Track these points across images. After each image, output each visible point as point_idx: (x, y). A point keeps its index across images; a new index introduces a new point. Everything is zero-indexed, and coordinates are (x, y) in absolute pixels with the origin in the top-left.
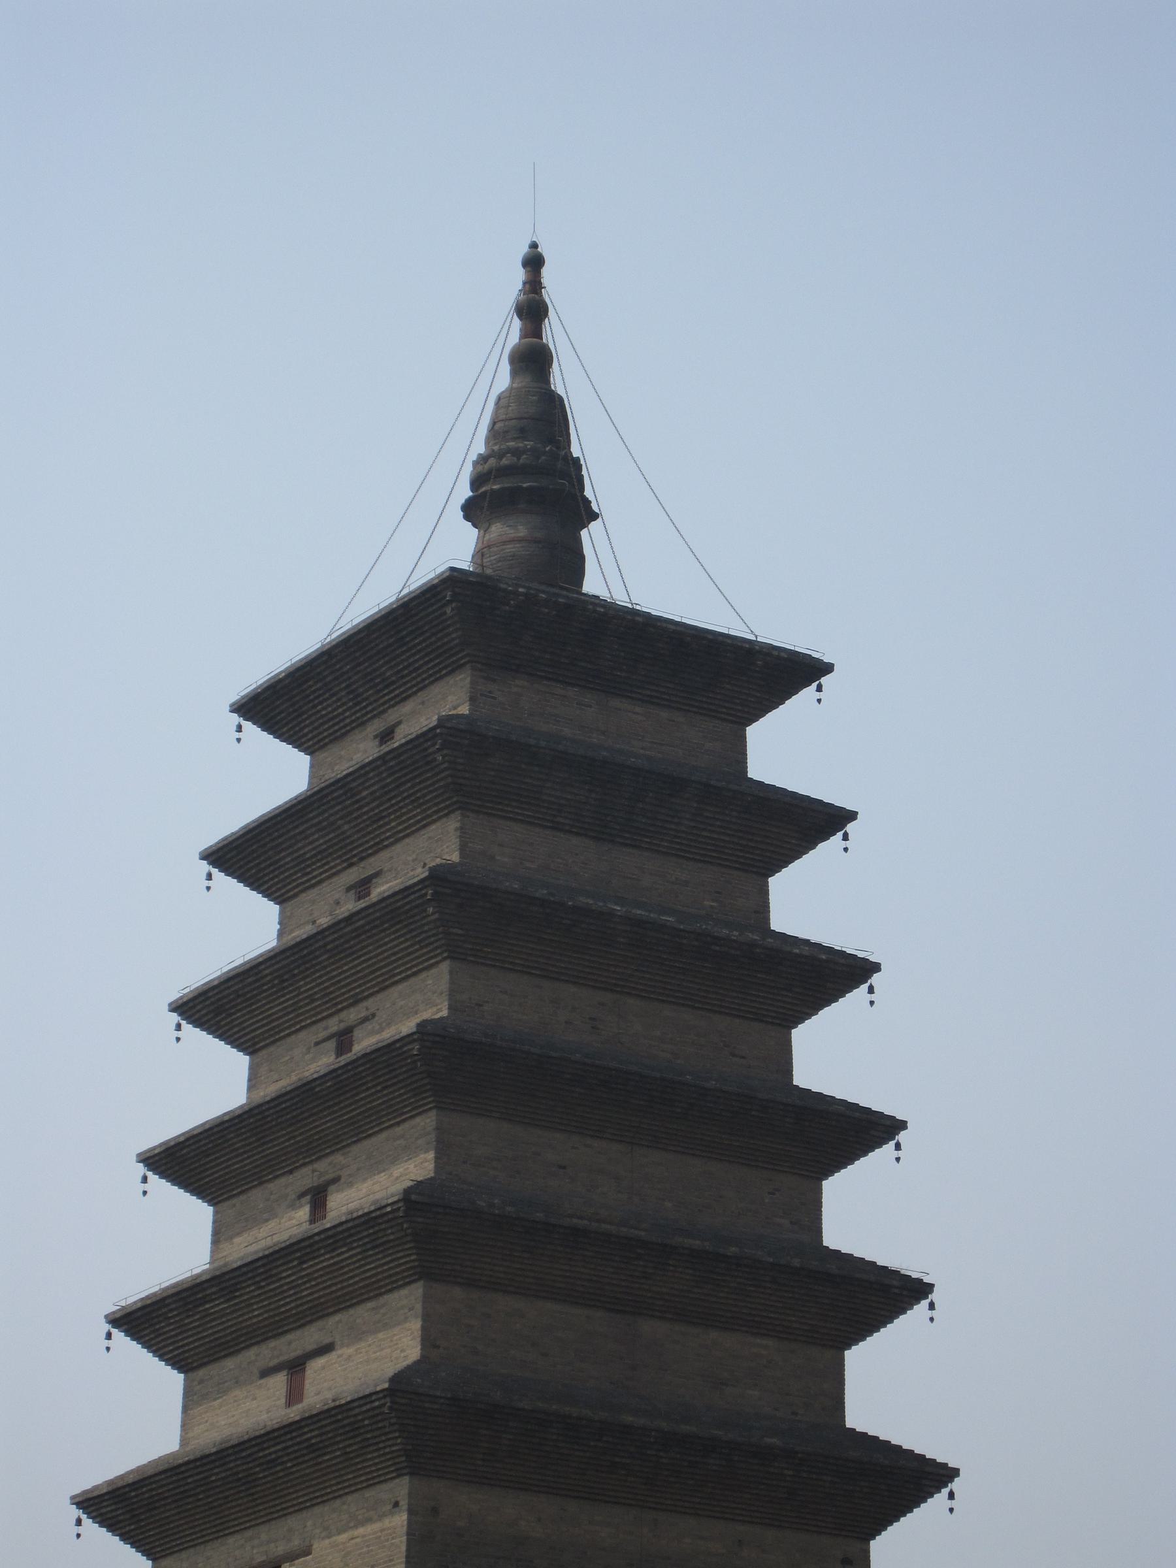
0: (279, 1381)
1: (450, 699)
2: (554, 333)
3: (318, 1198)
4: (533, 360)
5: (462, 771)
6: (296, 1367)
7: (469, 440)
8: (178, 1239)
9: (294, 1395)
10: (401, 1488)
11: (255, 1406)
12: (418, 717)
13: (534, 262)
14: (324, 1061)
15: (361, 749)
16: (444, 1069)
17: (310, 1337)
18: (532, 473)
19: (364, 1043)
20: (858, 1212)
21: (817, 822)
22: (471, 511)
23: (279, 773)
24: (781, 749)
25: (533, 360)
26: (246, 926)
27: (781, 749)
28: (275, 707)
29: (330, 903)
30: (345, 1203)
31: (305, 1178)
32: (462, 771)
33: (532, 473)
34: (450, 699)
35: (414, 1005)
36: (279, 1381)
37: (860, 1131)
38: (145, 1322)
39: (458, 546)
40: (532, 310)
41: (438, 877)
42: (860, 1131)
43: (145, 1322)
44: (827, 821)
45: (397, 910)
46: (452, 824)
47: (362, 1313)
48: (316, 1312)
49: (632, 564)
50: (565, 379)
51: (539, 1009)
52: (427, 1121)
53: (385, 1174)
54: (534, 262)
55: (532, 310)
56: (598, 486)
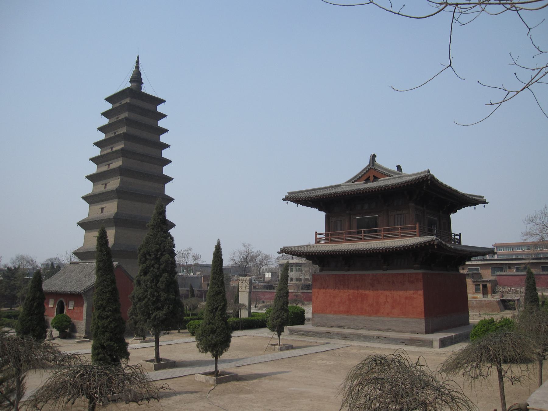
0: (107, 166)
1: (128, 100)
2: (140, 65)
3: (112, 149)
4: (137, 67)
5: (129, 107)
6: (109, 165)
7: (131, 75)
8: (93, 169)
9: (105, 187)
10: (119, 177)
11: (104, 168)
12: (124, 102)
13: (138, 57)
14: (113, 135)
15: (118, 105)
16: (126, 137)
17: (110, 162)
18: (137, 79)
19: (117, 133)
20: (165, 154)
21: (164, 116)
22: (130, 82)
23: (109, 106)
24: (160, 109)
25: (137, 67)
26: (105, 121)
27: (160, 109)
28: (109, 99)
29: (114, 120)
30: (114, 149)
31: (110, 146)
32: (129, 107)
33: (137, 79)
34: (128, 100)
35: (122, 130)
36: (107, 166)
37: (166, 146)
38: (94, 160)
39: (129, 85)
40: (138, 62)
41: (125, 118)
42: (166, 146)
43: (94, 160)
44: (165, 116)
45: (121, 120)
46: (129, 98)
47: (116, 160)
48: (111, 159)
49: (146, 89)
50: (141, 69)
51: (135, 116)
52: (123, 142)
53: (118, 147)
54: (138, 57)
55: (138, 62)
56: (143, 81)
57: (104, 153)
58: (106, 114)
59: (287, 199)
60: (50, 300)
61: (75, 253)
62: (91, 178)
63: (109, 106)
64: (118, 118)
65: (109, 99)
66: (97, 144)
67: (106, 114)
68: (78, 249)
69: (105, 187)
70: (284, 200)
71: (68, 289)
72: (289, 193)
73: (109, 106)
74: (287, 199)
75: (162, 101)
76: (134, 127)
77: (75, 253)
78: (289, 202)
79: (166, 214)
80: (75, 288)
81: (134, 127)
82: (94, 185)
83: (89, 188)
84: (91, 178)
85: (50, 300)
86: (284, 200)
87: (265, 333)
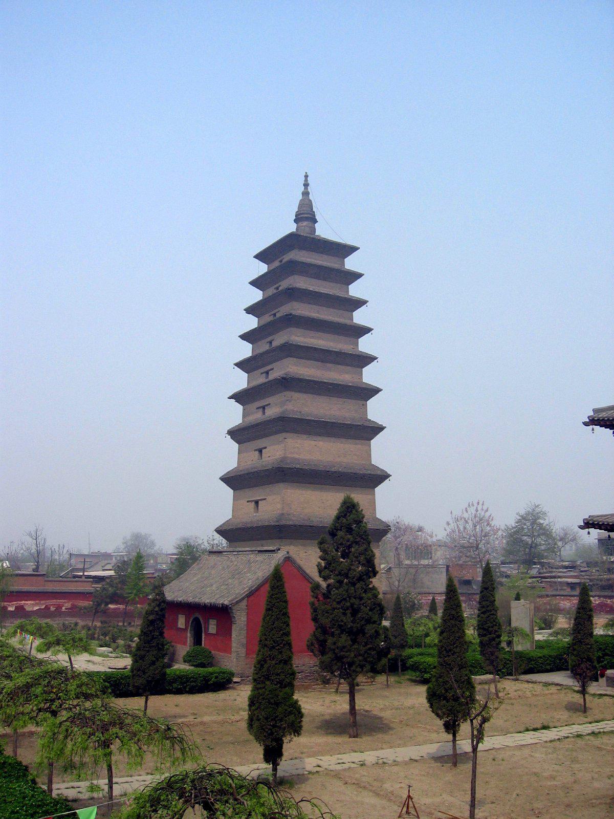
4: (306, 194)
6: (267, 373)
8: (241, 381)
13: (306, 176)
14: (272, 318)
15: (276, 264)
18: (306, 215)
24: (351, 263)
25: (306, 194)
27: (351, 263)
28: (262, 256)
29: (268, 318)
33: (306, 215)
40: (306, 185)
49: (323, 231)
54: (306, 176)
55: (306, 185)
57: (263, 323)
58: (251, 310)
59: (593, 421)
60: (180, 616)
61: (219, 531)
62: (238, 397)
63: (262, 268)
64: (277, 288)
65: (262, 256)
66: (245, 337)
67: (251, 310)
68: (221, 526)
69: (264, 413)
70: (586, 424)
71: (206, 599)
72: (595, 411)
73: (262, 268)
74: (593, 421)
75: (350, 250)
76: (305, 299)
77: (219, 531)
78: (597, 428)
79: (383, 520)
80: (217, 596)
81: (305, 299)
82: (244, 410)
83: (235, 415)
84: (238, 397)
85: (180, 616)
86: (586, 424)
87: (561, 678)
